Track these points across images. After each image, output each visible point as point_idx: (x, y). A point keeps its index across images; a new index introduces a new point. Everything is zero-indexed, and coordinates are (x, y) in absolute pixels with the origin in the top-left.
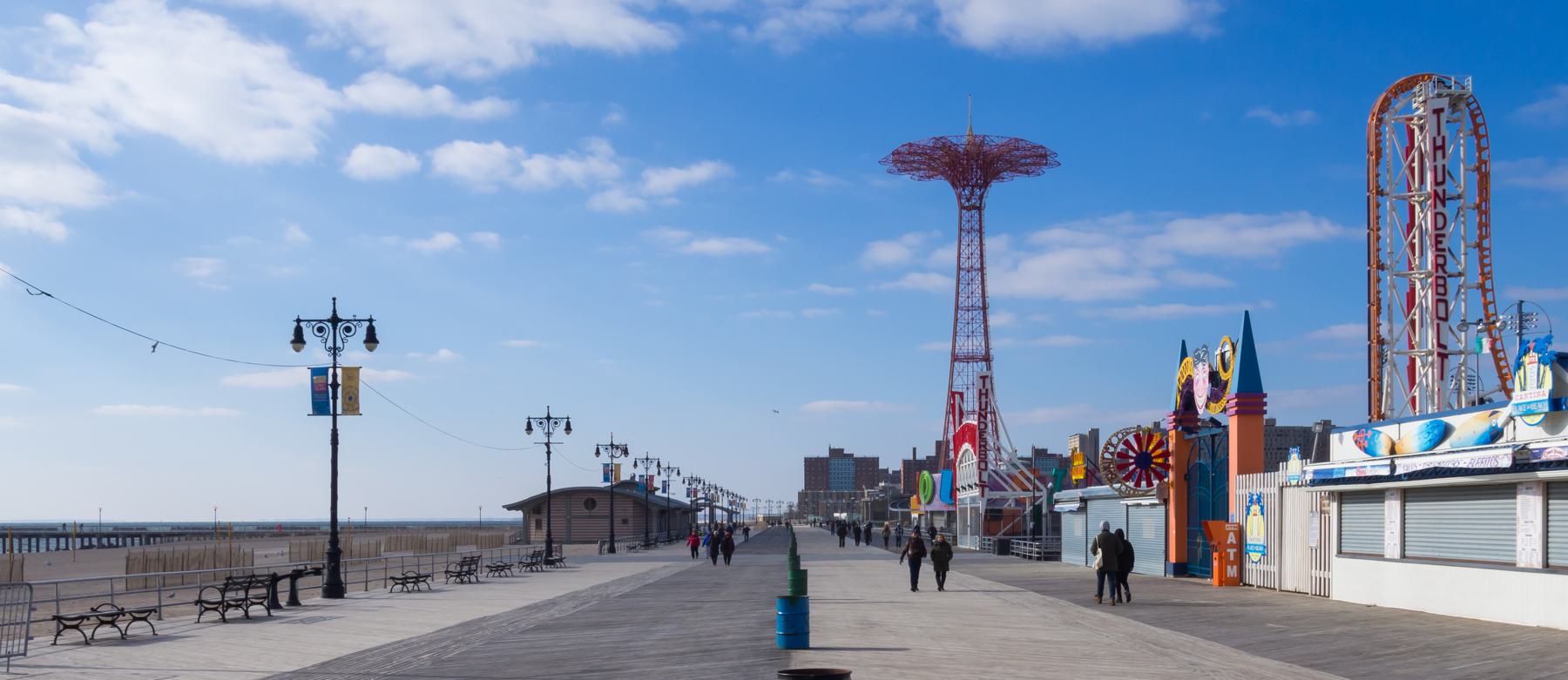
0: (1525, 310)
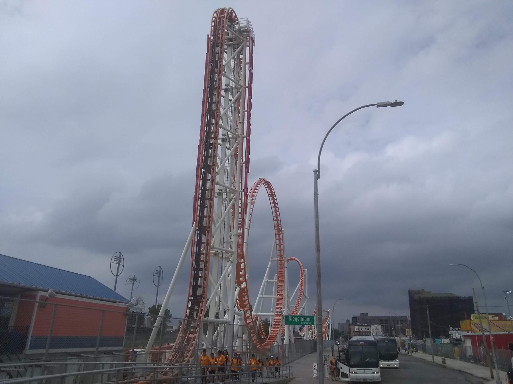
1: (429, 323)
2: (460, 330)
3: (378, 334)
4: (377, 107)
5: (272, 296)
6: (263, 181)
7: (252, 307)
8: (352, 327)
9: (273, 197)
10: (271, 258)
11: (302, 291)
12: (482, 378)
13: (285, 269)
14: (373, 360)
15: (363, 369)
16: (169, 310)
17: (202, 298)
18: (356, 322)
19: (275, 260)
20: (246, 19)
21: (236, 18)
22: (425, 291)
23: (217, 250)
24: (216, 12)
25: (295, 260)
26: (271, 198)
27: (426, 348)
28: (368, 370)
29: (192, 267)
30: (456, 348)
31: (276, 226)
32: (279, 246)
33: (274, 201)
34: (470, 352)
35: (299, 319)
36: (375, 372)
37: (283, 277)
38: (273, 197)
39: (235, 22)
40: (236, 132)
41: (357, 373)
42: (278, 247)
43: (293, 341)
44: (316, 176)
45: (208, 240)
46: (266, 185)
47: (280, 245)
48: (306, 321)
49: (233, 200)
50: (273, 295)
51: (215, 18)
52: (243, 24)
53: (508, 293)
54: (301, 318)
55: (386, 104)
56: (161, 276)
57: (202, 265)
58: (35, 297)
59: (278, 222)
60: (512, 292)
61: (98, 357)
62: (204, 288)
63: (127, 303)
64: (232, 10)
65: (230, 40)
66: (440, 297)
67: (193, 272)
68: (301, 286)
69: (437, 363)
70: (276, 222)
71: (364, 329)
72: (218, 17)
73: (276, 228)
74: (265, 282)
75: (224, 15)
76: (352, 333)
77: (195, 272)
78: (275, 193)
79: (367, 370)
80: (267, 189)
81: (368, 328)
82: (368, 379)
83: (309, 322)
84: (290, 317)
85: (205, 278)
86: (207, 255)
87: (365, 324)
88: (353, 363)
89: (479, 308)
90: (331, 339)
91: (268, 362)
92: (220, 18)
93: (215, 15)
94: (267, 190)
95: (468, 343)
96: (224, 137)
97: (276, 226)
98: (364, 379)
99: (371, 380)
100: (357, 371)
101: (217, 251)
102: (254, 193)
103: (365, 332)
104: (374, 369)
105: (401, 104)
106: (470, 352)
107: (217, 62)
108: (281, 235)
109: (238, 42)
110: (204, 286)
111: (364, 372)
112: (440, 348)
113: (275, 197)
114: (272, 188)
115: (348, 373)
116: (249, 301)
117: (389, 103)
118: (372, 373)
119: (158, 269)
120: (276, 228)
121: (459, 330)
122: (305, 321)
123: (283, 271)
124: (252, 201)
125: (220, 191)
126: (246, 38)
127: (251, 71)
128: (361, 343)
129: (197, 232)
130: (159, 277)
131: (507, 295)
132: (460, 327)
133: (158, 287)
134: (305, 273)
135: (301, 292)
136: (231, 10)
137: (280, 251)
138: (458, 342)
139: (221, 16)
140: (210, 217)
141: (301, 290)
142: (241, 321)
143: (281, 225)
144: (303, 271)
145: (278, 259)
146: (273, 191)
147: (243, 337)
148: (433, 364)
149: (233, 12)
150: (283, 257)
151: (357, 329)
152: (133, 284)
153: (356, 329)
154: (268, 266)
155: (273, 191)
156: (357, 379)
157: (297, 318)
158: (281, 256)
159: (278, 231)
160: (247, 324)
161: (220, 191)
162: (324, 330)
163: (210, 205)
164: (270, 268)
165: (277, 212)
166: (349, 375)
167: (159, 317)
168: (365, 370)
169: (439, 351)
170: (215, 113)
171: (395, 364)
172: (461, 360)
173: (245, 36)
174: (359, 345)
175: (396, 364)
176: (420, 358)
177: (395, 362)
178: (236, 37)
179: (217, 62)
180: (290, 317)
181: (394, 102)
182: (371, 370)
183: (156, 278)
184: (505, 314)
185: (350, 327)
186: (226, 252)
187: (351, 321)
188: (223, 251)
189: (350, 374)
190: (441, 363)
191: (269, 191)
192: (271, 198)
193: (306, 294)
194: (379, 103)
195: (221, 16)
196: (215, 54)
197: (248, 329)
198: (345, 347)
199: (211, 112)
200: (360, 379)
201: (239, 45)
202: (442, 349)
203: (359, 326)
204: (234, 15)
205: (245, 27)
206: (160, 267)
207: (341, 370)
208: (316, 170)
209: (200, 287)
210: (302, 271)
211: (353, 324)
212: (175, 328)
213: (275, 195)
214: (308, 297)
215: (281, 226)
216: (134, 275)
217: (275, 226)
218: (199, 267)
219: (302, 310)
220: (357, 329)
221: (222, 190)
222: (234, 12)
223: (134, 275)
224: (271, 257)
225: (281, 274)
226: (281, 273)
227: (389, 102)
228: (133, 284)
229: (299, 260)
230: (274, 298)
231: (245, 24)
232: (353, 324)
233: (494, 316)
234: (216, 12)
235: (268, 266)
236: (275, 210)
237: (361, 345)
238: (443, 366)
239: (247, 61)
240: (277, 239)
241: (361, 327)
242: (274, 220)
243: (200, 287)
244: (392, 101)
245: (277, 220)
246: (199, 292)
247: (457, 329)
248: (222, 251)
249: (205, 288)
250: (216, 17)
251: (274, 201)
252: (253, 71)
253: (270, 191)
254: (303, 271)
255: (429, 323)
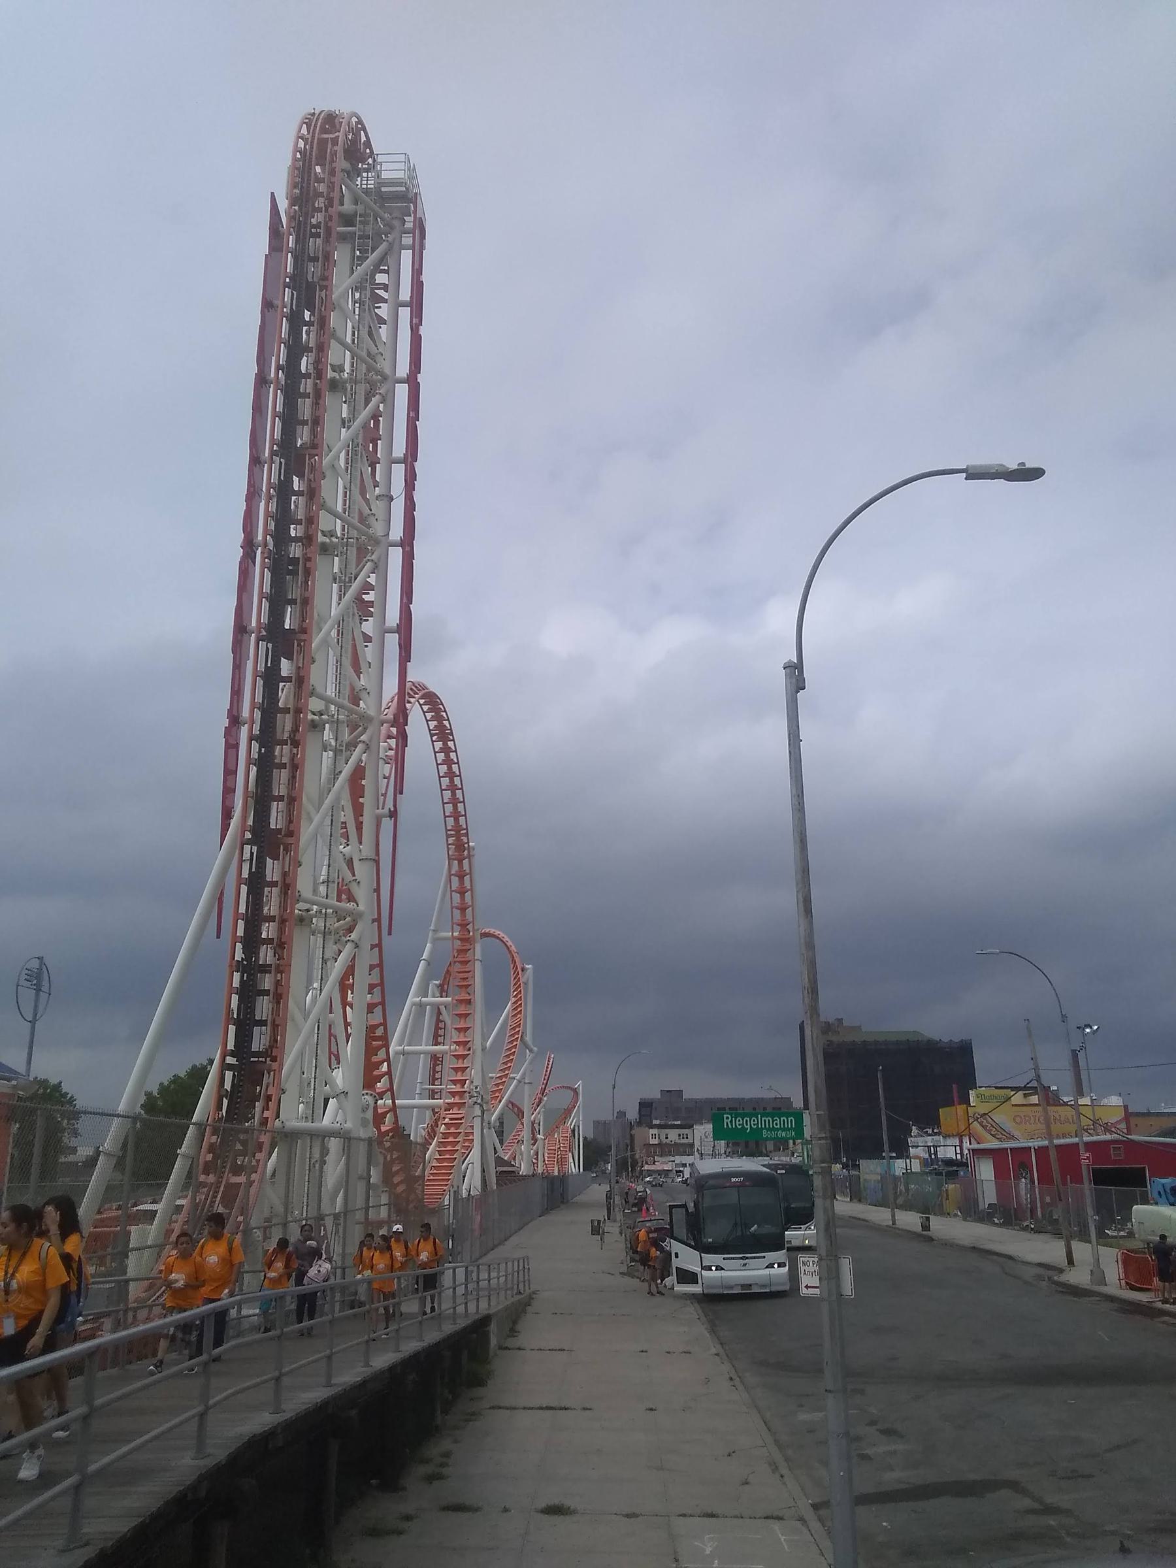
1: (884, 1118)
2: (939, 1134)
4: (966, 479)
5: (420, 1047)
6: (419, 690)
8: (638, 1132)
9: (445, 744)
10: (434, 930)
11: (517, 1030)
12: (1040, 1265)
13: (478, 965)
14: (768, 1229)
15: (741, 1256)
16: (72, 1097)
17: (268, 1059)
18: (650, 1115)
19: (445, 939)
20: (402, 158)
21: (368, 151)
22: (845, 1023)
23: (307, 906)
24: (307, 121)
25: (498, 938)
26: (438, 745)
27: (862, 1186)
28: (755, 1258)
29: (231, 962)
30: (951, 1187)
31: (453, 833)
33: (447, 756)
34: (989, 1195)
35: (741, 1122)
36: (774, 1264)
37: (469, 990)
38: (445, 744)
39: (363, 161)
40: (369, 527)
41: (722, 1269)
42: (457, 897)
43: (493, 1179)
44: (794, 680)
45: (285, 874)
46: (425, 704)
47: (462, 893)
48: (778, 1130)
49: (360, 747)
50: (423, 1043)
51: (306, 141)
52: (391, 170)
53: (1088, 1030)
54: (763, 1119)
55: (994, 471)
56: (45, 988)
57: (266, 955)
59: (457, 820)
60: (1098, 1028)
62: (275, 1026)
63: (9, 1080)
64: (360, 122)
65: (348, 220)
66: (876, 1042)
67: (237, 976)
68: (515, 1015)
69: (902, 1230)
70: (451, 821)
71: (673, 1135)
72: (316, 138)
73: (451, 840)
74: (414, 1004)
75: (337, 134)
76: (637, 1149)
77: (242, 977)
78: (451, 729)
79: (751, 1258)
80: (429, 715)
81: (687, 1135)
82: (757, 1284)
83: (788, 1129)
84: (727, 1118)
85: (279, 997)
86: (283, 921)
87: (676, 1123)
88: (710, 1240)
89: (1042, 1073)
90: (581, 1170)
91: (430, 1246)
92: (323, 143)
93: (304, 130)
94: (427, 721)
95: (986, 1171)
96: (328, 540)
97: (453, 833)
98: (743, 1286)
99: (764, 1286)
100: (723, 1264)
101: (308, 910)
102: (391, 729)
104: (772, 1256)
105: (1034, 474)
106: (989, 1195)
107: (311, 287)
108: (466, 862)
109: (373, 229)
110: (274, 1021)
111: (745, 1265)
112: (903, 1188)
113: (450, 744)
114: (444, 714)
115: (698, 1269)
116: (389, 1066)
117: (1001, 469)
118: (767, 1267)
119: (35, 964)
120: (451, 840)
121: (935, 1134)
122: (774, 1129)
123: (469, 972)
124: (386, 754)
125: (316, 718)
126: (400, 218)
127: (418, 330)
128: (733, 1180)
129: (247, 848)
130: (38, 990)
131: (1085, 1035)
132: (939, 1126)
133: (33, 1022)
134: (526, 976)
135: (515, 1031)
136: (354, 119)
137: (463, 909)
138: (953, 1169)
139: (326, 136)
140: (292, 800)
141: (514, 1029)
143: (467, 829)
144: (519, 970)
145: (456, 934)
146: (448, 725)
147: (369, 1176)
148: (892, 1230)
149: (361, 129)
150: (471, 929)
151: (654, 1136)
153: (653, 1136)
154: (424, 957)
155: (446, 723)
156: (722, 1287)
157: (748, 1119)
158: (464, 926)
159: (455, 849)
160: (382, 1135)
161: (316, 718)
162: (563, 1144)
163: (293, 760)
164: (429, 963)
165: (457, 791)
166: (699, 1276)
167: (194, 1124)
168: (747, 1258)
169: (901, 1194)
170: (307, 456)
171: (804, 1237)
172: (965, 1219)
173: (396, 214)
174: (729, 1187)
175: (810, 1237)
176: (850, 1217)
177: (806, 1230)
178: (368, 211)
179: (311, 287)
180: (727, 1118)
181: (1016, 467)
182: (764, 1257)
183: (28, 995)
184: (1055, 1088)
185: (633, 1132)
186: (336, 913)
187: (633, 1114)
188: (328, 911)
189: (703, 1271)
190: (919, 1229)
191: (433, 724)
192: (438, 745)
193: (528, 1038)
194: (974, 467)
195: (326, 136)
196: (306, 261)
197: (384, 1152)
198: (640, 1192)
199: (293, 455)
200: (731, 1288)
201: (378, 238)
202: (907, 1190)
203: (659, 1127)
204: (363, 138)
205: (400, 184)
206: (40, 959)
207: (675, 1263)
208: (793, 664)
209: (262, 1023)
210: (518, 971)
211: (639, 1124)
212: (84, 1152)
213: (451, 737)
214: (535, 1049)
215: (467, 835)
218: (257, 959)
219: (516, 1087)
220: (654, 1136)
221: (322, 715)
224: (432, 928)
225: (464, 979)
226: (462, 975)
227: (1002, 465)
229: (509, 937)
230: (425, 1053)
231: (400, 175)
232: (639, 1124)
233: (1031, 1095)
234: (309, 121)
235: (424, 957)
236: (450, 782)
237: (735, 1185)
238: (924, 1237)
239: (405, 294)
240: (453, 872)
241: (667, 1131)
242: (447, 814)
243: (262, 1023)
244: (1013, 465)
245: (456, 815)
246: (259, 1040)
247: (930, 1131)
248: (324, 911)
249: (278, 1026)
250: (309, 137)
251: (447, 756)
252: (423, 330)
253: (435, 723)
254: (519, 970)
255: (884, 1118)
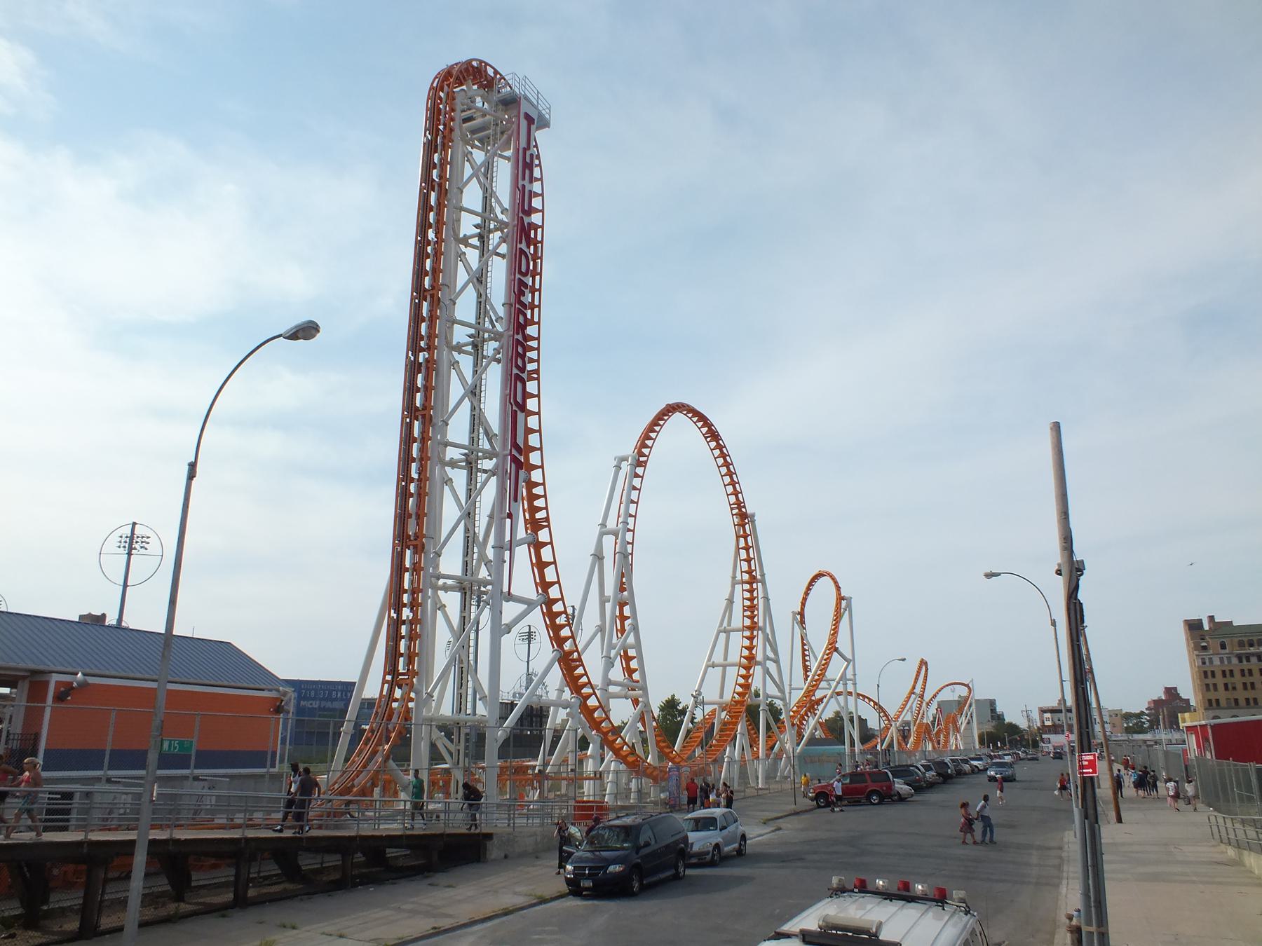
0: (138, 531)
3: (458, 729)
7: (1205, 689)
9: (718, 443)
26: (713, 444)
32: (745, 551)
38: (718, 443)
58: (47, 683)
61: (94, 808)
103: (1080, 735)
142: (572, 718)
152: (529, 644)
191: (705, 430)
216: (530, 626)
217: (732, 506)
222: (487, 64)
223: (530, 626)
228: (529, 644)
